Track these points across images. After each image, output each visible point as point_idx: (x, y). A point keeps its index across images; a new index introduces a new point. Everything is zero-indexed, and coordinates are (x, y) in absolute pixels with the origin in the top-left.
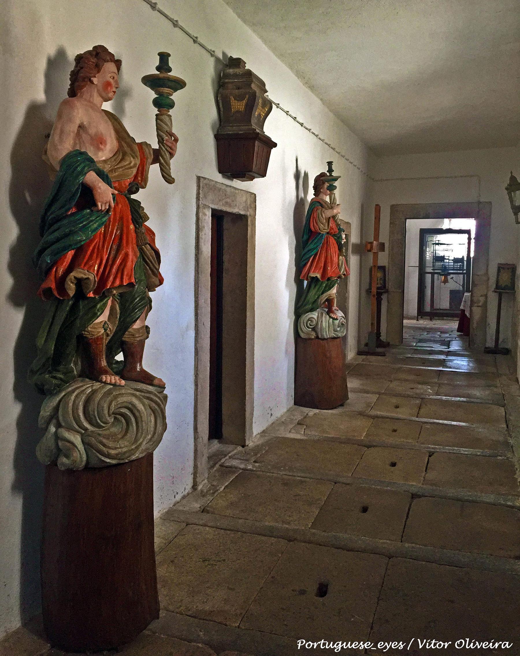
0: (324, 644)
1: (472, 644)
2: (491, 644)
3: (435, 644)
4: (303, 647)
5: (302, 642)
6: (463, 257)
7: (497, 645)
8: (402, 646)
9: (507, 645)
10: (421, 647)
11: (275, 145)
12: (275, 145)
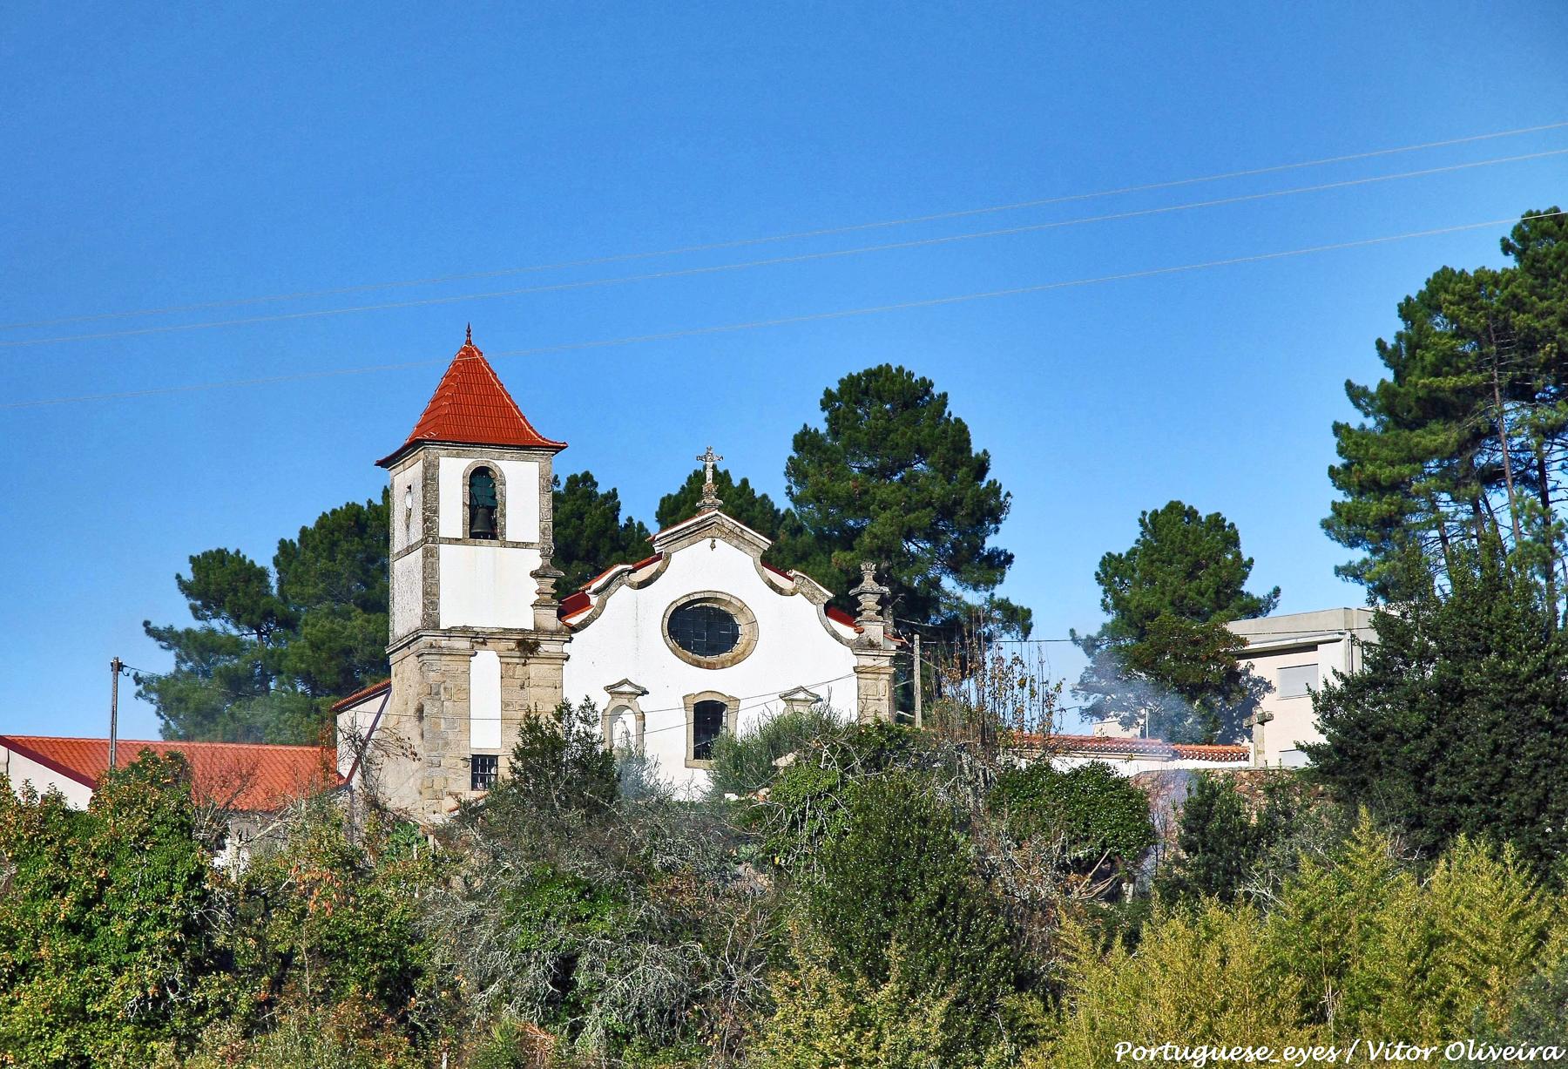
0: (1171, 1053)
1: (1481, 1051)
2: (1520, 1051)
3: (1403, 1051)
4: (1126, 1057)
5: (1125, 1047)
6: (1338, 429)
7: (1532, 1054)
8: (1334, 1056)
9: (1554, 1054)
10: (1373, 1057)
11: (192, 559)
12: (192, 559)
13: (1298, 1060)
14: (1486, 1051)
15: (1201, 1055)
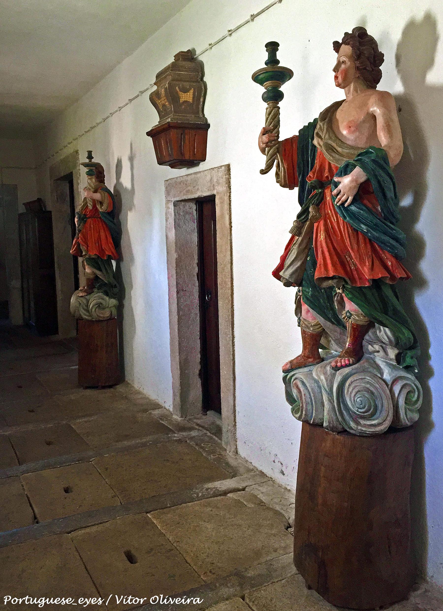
0: (29, 600)
1: (166, 600)
3: (131, 600)
5: (8, 598)
7: (188, 601)
8: (101, 602)
9: (198, 601)
10: (118, 603)
13: (85, 603)
14: (168, 599)
15: (42, 602)
